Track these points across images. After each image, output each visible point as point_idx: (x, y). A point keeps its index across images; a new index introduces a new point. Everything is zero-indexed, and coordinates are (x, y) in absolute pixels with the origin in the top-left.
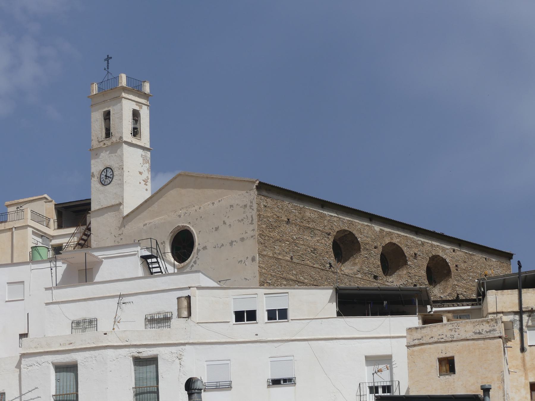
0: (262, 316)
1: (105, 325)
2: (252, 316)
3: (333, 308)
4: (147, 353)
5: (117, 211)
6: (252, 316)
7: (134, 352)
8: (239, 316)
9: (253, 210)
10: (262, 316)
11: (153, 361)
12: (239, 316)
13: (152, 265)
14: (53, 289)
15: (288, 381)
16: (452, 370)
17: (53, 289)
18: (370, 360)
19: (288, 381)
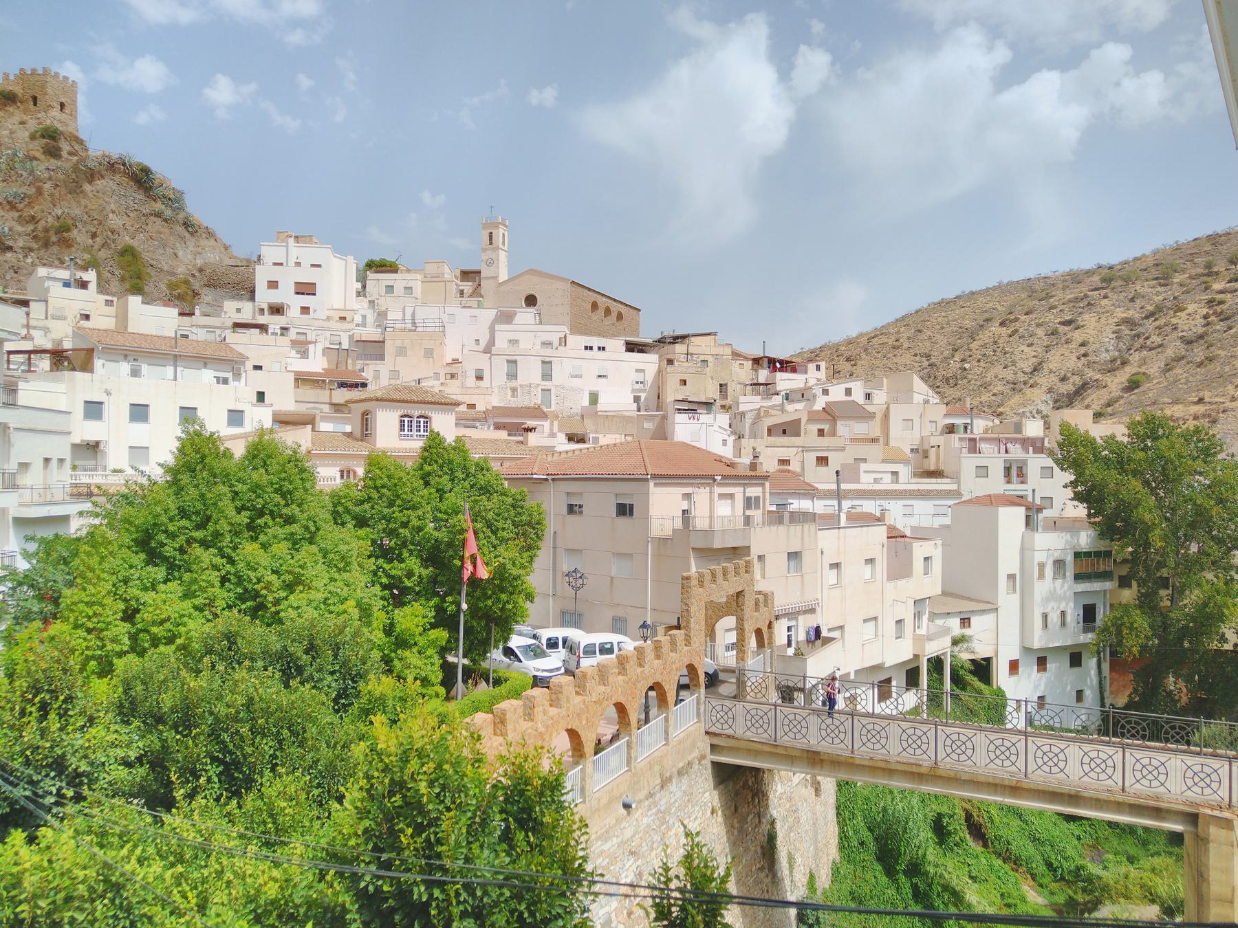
0: (595, 348)
1: (522, 345)
2: (591, 348)
3: (624, 348)
4: (548, 359)
5: (983, 829)
6: (591, 348)
7: (543, 359)
8: (586, 348)
9: (312, 665)
10: (595, 348)
11: (550, 362)
12: (586, 348)
13: (47, 487)
14: (472, 866)
15: (319, 266)
16: (685, 384)
17: (472, 866)
18: (637, 371)
19: (319, 266)
